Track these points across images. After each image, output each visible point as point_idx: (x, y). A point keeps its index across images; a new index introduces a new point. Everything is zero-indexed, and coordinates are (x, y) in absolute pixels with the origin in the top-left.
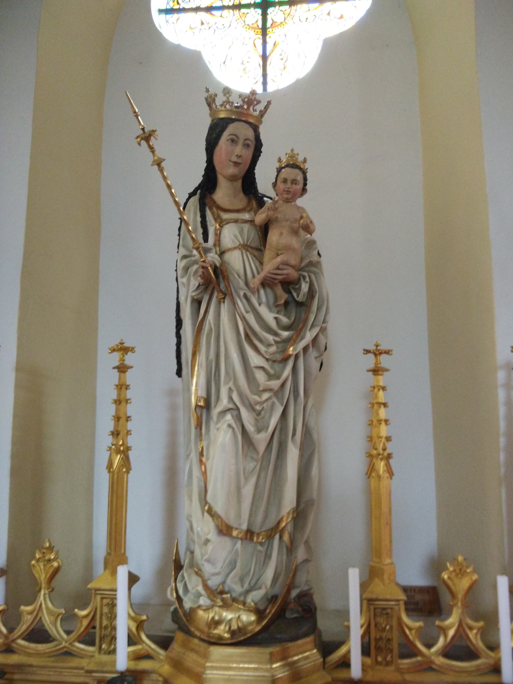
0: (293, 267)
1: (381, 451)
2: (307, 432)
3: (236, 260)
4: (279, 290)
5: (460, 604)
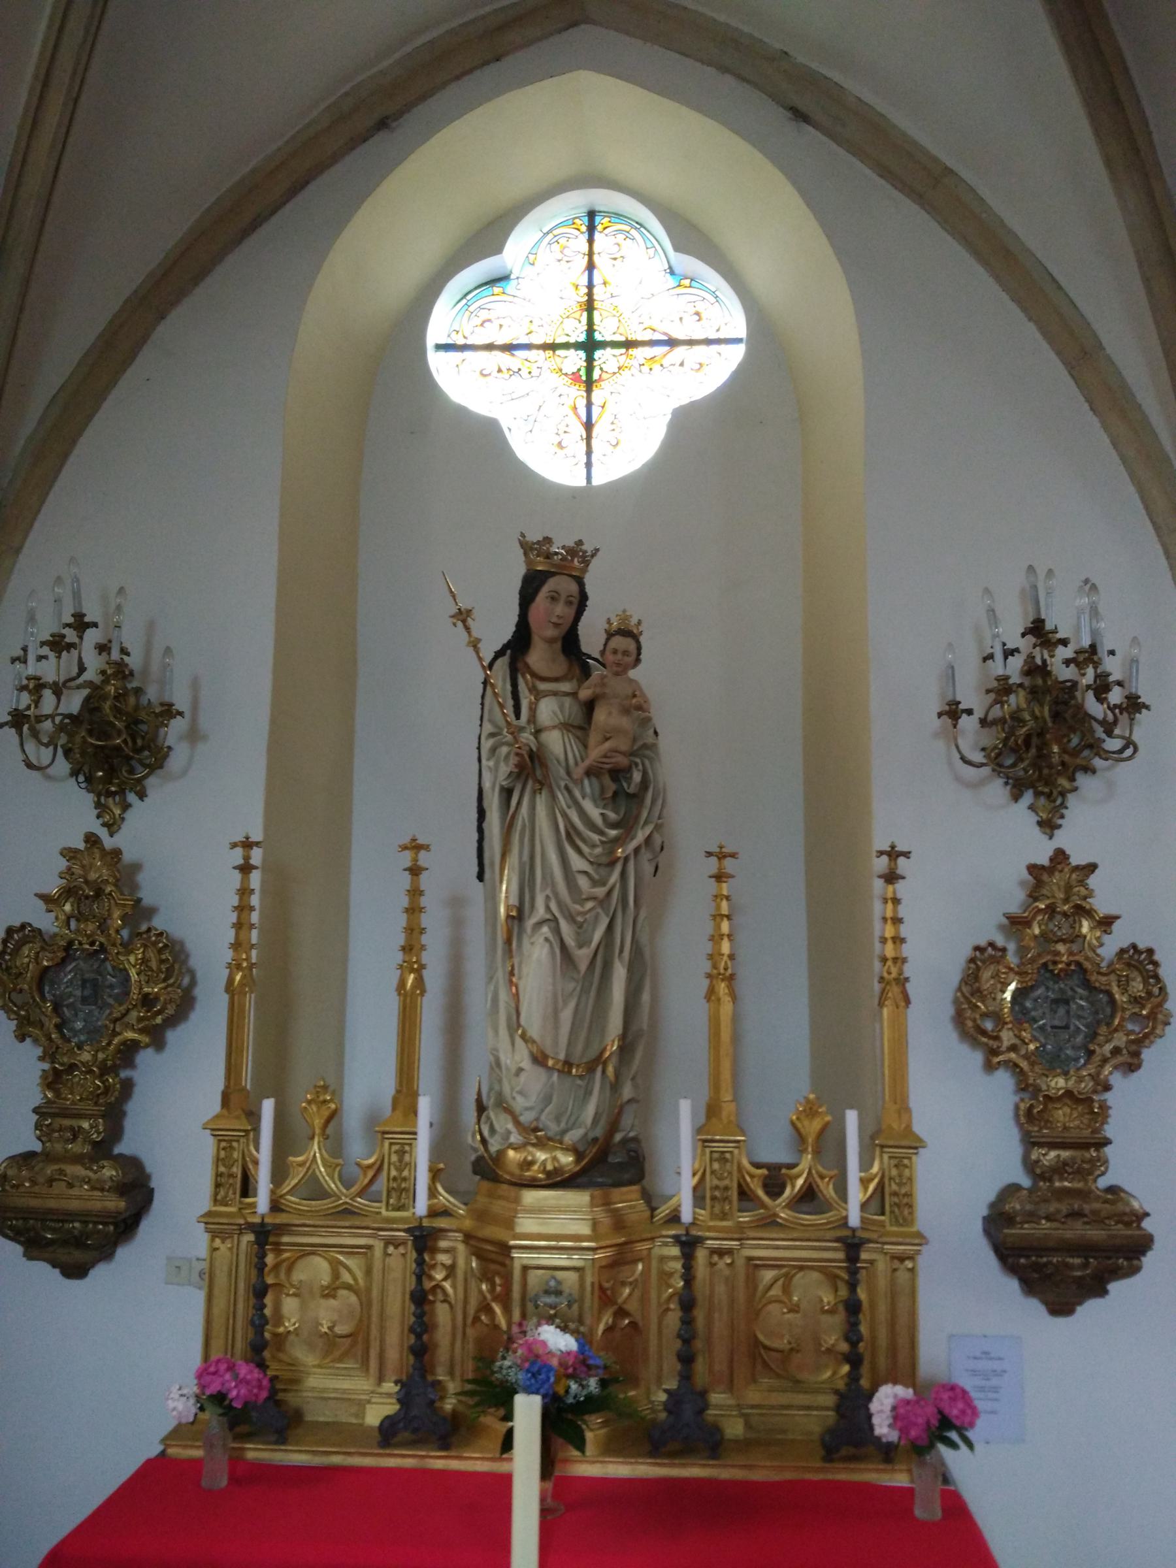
0: (623, 753)
1: (722, 971)
2: (637, 951)
3: (556, 743)
4: (607, 780)
5: (810, 1149)
